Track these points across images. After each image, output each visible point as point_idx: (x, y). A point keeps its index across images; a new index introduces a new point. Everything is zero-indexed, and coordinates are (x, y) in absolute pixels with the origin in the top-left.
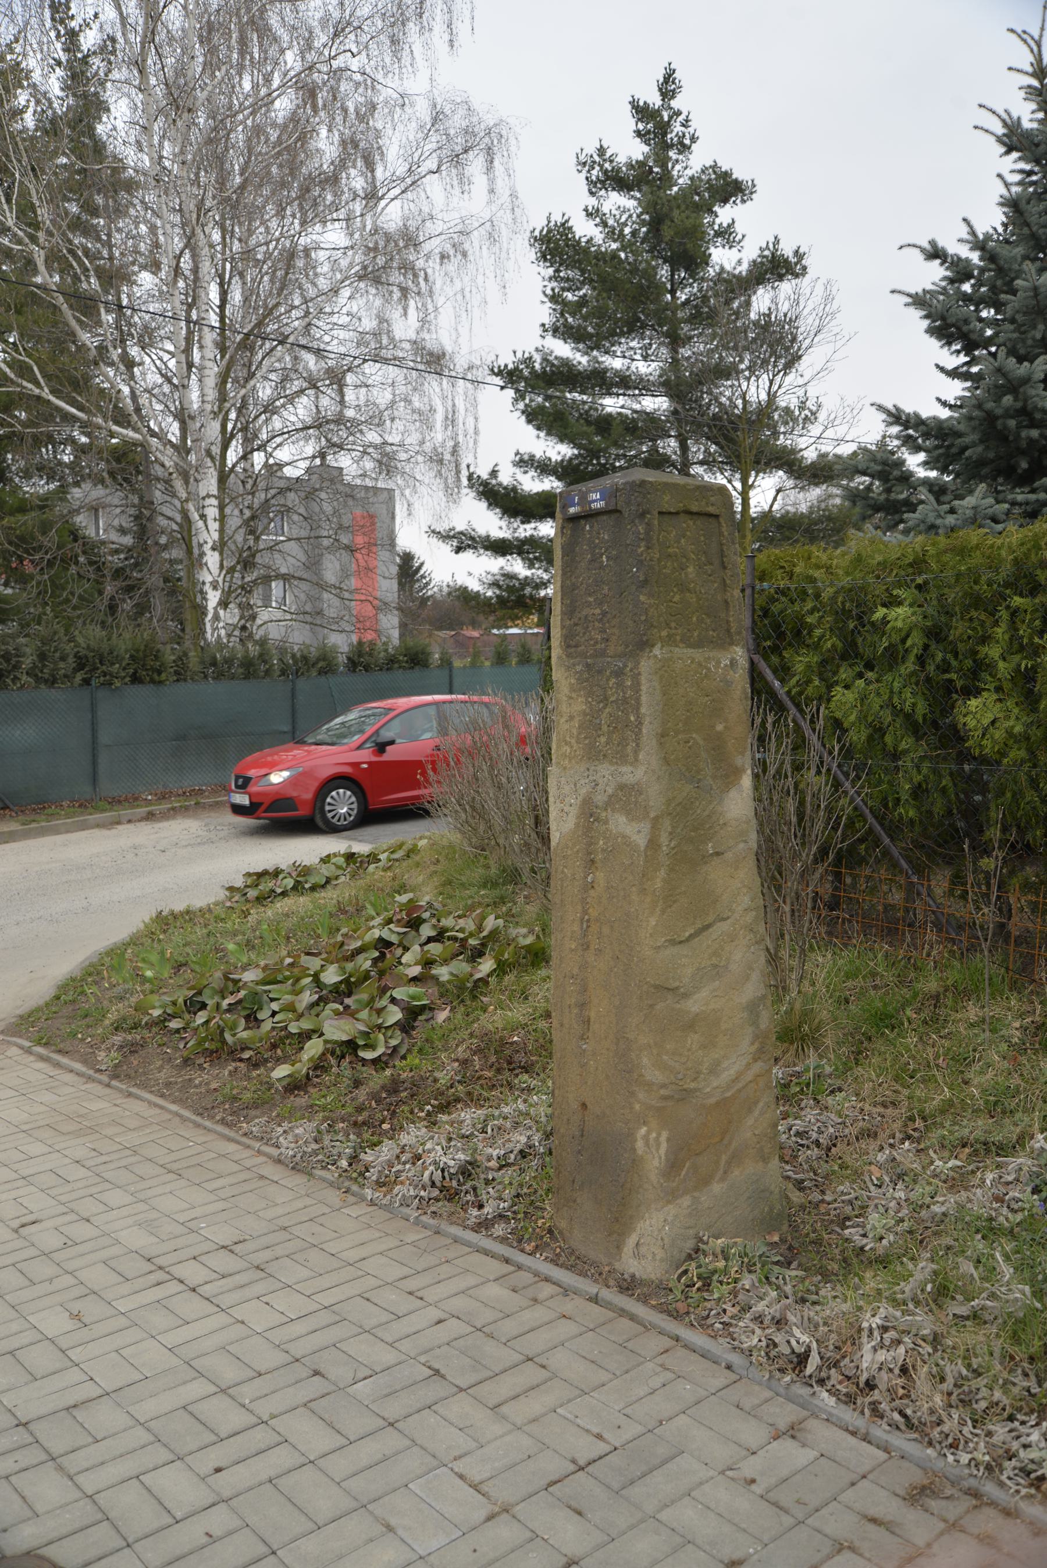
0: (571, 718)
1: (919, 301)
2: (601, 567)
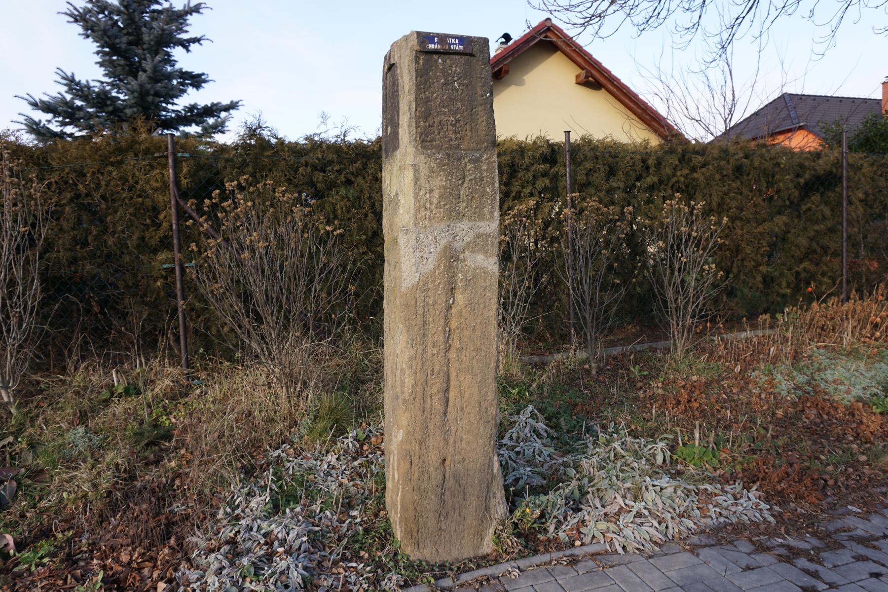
0: (431, 191)
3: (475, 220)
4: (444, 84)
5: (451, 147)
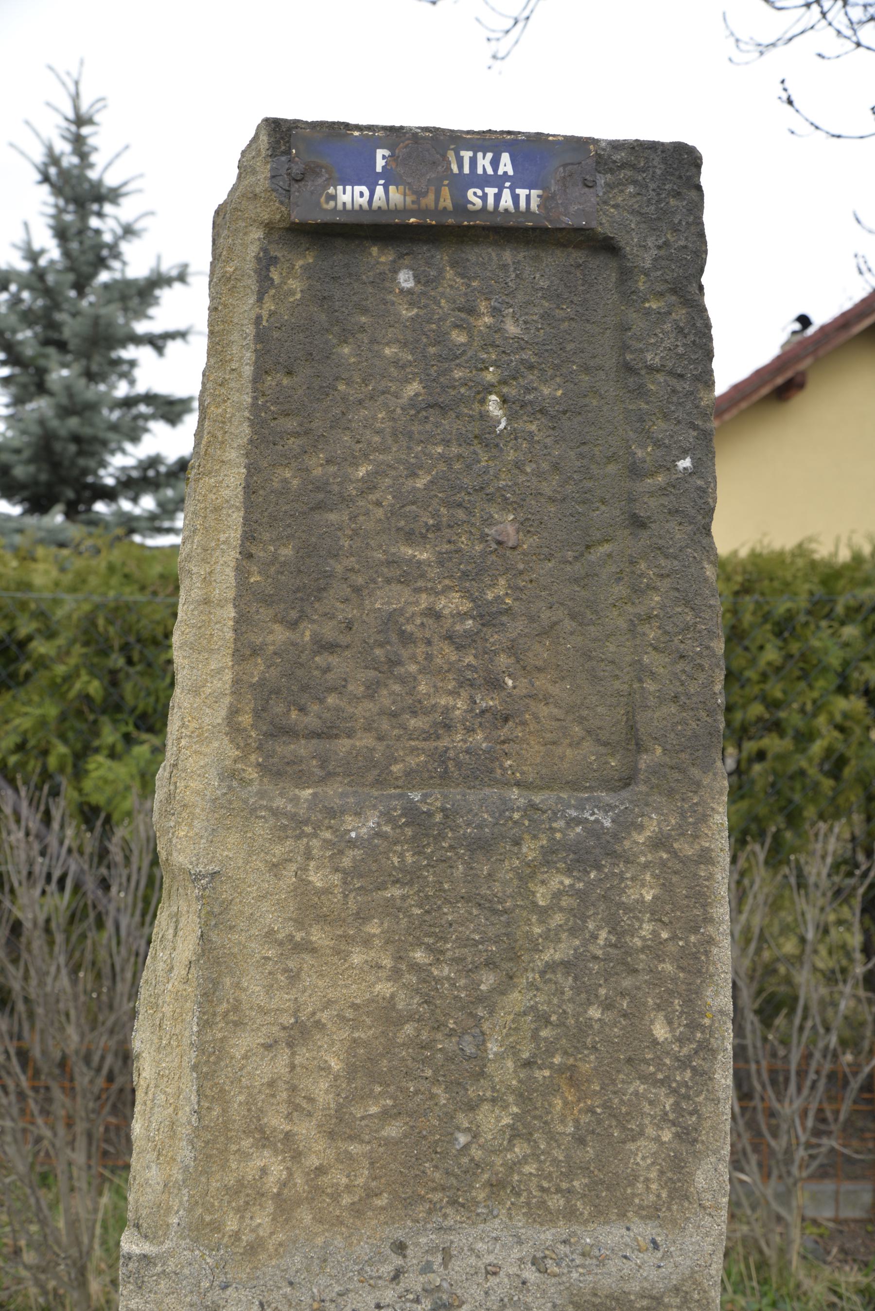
0: (300, 1033)
2: (485, 436)
3: (570, 1214)
4: (424, 408)
5: (441, 770)
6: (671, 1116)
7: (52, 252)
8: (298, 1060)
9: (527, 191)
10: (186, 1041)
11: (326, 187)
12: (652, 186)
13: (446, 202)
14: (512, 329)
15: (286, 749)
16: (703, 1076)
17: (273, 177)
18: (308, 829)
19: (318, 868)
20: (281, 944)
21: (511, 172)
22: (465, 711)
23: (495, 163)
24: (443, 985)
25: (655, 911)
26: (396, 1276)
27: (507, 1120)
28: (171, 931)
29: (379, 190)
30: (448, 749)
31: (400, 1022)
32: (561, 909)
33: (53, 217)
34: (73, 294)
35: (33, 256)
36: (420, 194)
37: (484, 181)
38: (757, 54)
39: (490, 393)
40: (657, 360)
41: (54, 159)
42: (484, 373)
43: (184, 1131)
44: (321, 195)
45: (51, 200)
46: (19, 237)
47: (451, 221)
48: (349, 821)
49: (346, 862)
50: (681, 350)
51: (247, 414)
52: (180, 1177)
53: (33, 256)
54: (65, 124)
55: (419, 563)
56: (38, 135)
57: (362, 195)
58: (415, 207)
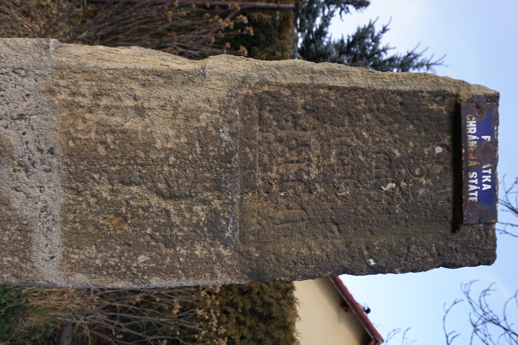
0: (140, 111)
1: (371, 26)
3: (65, 222)
5: (247, 167)
6: (106, 264)
7: (385, 57)
8: (129, 110)
9: (476, 195)
10: (137, 65)
11: (475, 116)
12: (480, 246)
13: (472, 164)
14: (421, 191)
15: (254, 104)
16: (122, 276)
17: (478, 96)
18: (223, 112)
19: (208, 117)
20: (177, 102)
21: (483, 189)
22: (271, 177)
23: (487, 183)
24: (160, 168)
25: (191, 256)
26: (40, 150)
27: (104, 195)
28: (179, 62)
29: (475, 137)
30: (256, 170)
31: (145, 152)
32: (191, 216)
33: (397, 57)
34: (371, 63)
35: (385, 50)
36: (474, 153)
37: (480, 178)
38: (464, 291)
39: (396, 184)
40: (412, 250)
41: (416, 57)
42: (403, 181)
43: (100, 64)
44: (471, 114)
45: (402, 56)
46: (391, 46)
47: (464, 166)
48: (227, 129)
49: (210, 129)
50: (417, 259)
51: (385, 87)
52: (81, 62)
53: (385, 50)
54: (427, 60)
55: (329, 157)
56: (424, 51)
57: (473, 130)
58: (469, 151)
